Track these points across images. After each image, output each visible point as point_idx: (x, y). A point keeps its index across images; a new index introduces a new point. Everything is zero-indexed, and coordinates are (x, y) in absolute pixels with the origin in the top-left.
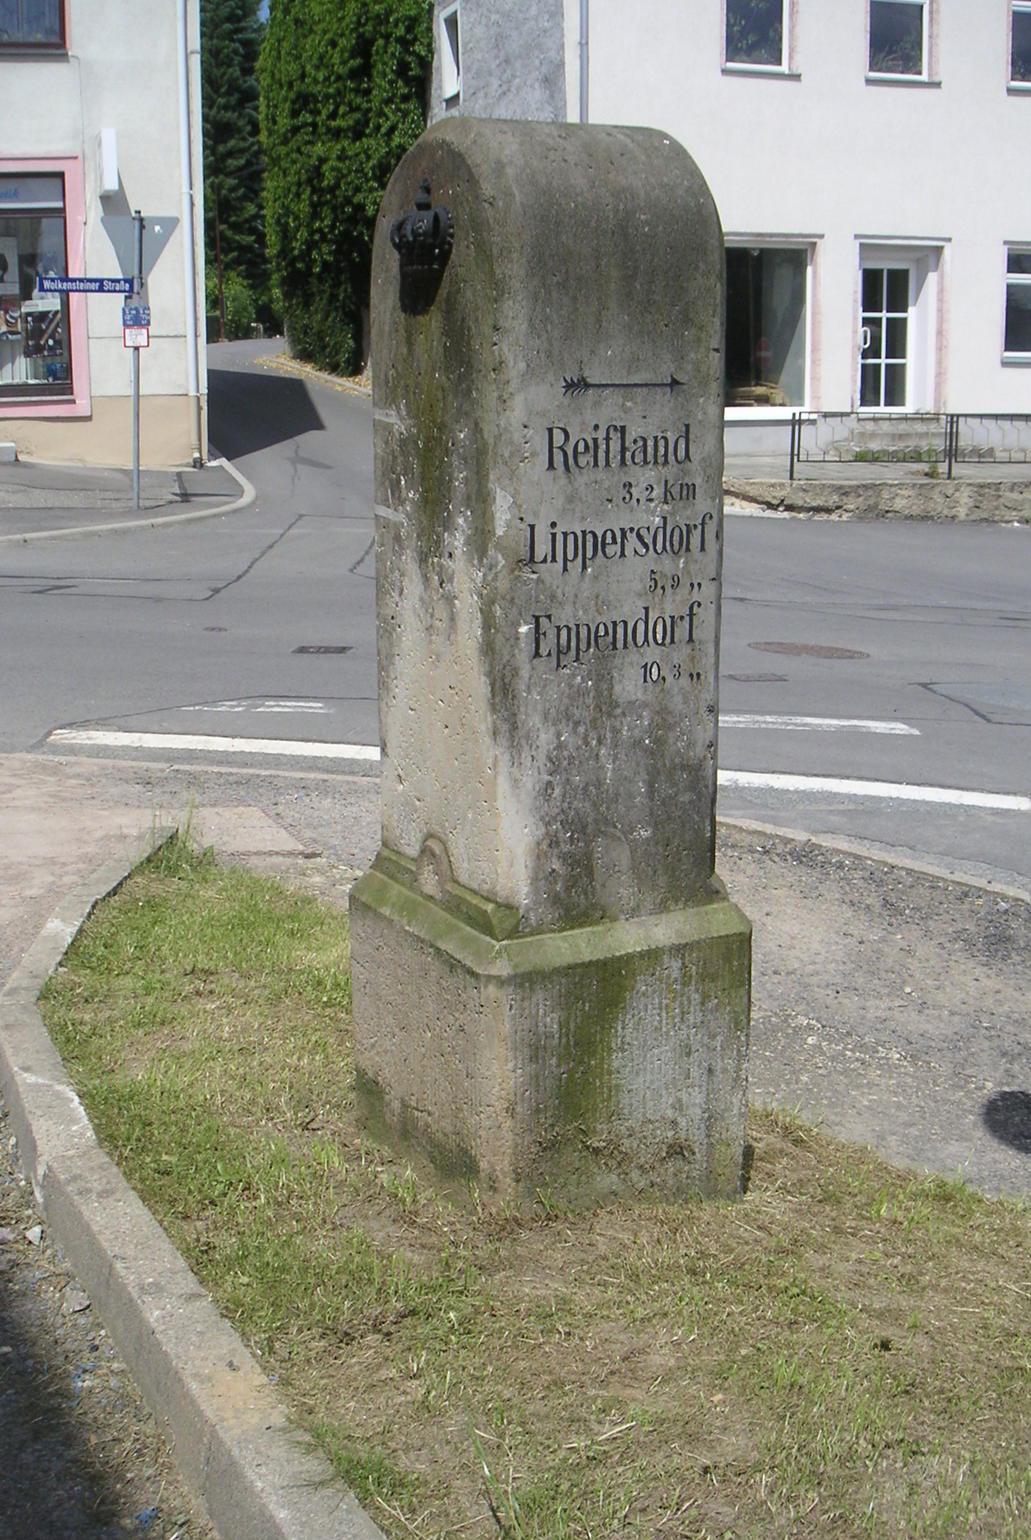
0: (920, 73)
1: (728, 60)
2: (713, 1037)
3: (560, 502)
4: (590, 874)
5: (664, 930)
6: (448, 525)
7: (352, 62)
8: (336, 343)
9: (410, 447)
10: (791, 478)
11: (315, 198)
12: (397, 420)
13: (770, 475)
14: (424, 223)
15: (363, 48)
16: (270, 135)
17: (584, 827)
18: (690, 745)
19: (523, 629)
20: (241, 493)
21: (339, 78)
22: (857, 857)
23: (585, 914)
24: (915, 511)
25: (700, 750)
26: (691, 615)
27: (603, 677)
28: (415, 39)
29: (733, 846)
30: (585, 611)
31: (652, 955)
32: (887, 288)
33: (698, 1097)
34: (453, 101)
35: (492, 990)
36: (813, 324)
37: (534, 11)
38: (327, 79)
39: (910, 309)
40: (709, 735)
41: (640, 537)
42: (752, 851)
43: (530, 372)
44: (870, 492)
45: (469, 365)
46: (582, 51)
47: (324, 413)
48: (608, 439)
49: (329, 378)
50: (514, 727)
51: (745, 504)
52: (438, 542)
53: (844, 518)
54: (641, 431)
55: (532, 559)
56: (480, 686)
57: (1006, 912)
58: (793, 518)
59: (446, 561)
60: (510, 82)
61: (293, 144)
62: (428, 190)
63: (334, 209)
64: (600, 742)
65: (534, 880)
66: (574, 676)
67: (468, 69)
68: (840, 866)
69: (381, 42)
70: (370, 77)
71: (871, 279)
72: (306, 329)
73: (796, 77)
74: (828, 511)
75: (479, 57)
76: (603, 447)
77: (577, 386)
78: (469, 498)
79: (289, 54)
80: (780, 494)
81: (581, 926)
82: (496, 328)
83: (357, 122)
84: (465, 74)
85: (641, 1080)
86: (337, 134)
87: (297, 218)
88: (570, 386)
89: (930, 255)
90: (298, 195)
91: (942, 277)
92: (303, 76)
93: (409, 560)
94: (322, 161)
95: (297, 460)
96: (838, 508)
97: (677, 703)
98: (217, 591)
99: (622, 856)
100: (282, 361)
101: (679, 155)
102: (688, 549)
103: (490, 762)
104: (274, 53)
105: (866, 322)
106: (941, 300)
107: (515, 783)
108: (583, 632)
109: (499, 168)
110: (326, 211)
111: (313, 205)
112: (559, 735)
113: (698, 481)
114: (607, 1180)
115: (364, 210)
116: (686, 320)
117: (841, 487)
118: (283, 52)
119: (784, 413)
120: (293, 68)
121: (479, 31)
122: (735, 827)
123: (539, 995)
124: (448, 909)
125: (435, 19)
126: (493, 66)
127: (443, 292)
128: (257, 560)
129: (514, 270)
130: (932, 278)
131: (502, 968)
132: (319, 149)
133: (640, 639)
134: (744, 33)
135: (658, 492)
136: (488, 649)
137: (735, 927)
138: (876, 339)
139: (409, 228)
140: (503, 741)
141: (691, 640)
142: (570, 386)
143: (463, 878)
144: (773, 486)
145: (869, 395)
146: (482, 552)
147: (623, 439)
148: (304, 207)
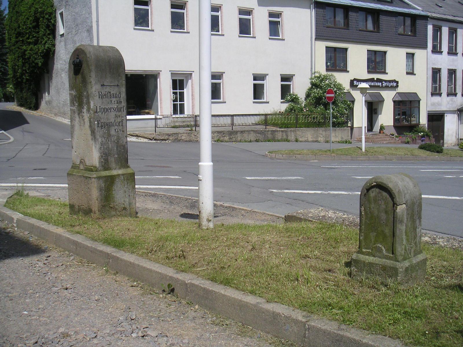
0: (184, 30)
1: (135, 26)
2: (129, 190)
3: (101, 103)
4: (108, 162)
5: (120, 172)
6: (83, 108)
7: (33, 24)
8: (31, 101)
9: (76, 96)
10: (155, 132)
11: (23, 61)
12: (74, 93)
13: (151, 132)
14: (78, 61)
15: (37, 20)
16: (9, 43)
17: (107, 154)
18: (123, 142)
19: (96, 123)
20: (10, 139)
21: (30, 28)
22: (165, 195)
23: (107, 168)
24: (187, 139)
25: (124, 143)
26: (122, 121)
27: (109, 131)
28: (51, 19)
29: (139, 195)
30: (105, 120)
31: (119, 175)
32: (178, 84)
33: (127, 200)
34: (62, 35)
35: (93, 180)
36: (160, 94)
37: (84, 12)
38: (26, 28)
39: (185, 89)
40: (126, 141)
41: (114, 109)
42: (142, 195)
43: (96, 83)
44: (176, 135)
45: (86, 83)
46: (97, 23)
47: (29, 120)
48: (108, 94)
49: (29, 111)
50: (95, 138)
51: (144, 139)
52: (81, 111)
53: (169, 142)
54: (113, 93)
55: (97, 112)
56: (89, 132)
57: (195, 202)
58: (156, 142)
59: (83, 114)
60: (78, 31)
61: (17, 46)
62: (78, 56)
63: (29, 64)
64: (108, 141)
65: (99, 163)
66: (104, 130)
67: (66, 27)
68: (161, 197)
69: (41, 19)
70: (39, 28)
71: (174, 82)
72: (22, 98)
73: (153, 31)
74: (165, 140)
75: (69, 24)
76: (107, 95)
77: (103, 85)
78: (86, 103)
79: (15, 21)
80: (153, 136)
81: (107, 170)
82: (90, 77)
83: (35, 40)
84: (66, 28)
85: (118, 196)
86: (29, 43)
87: (18, 66)
88: (102, 85)
89: (189, 75)
90: (18, 60)
91: (192, 81)
92: (19, 27)
93: (76, 115)
94: (25, 51)
95: (23, 131)
96: (168, 139)
97: (120, 135)
98: (9, 160)
99: (113, 159)
100: (14, 107)
101: (117, 51)
103: (91, 144)
104: (10, 20)
105: (174, 93)
106: (192, 87)
107: (96, 147)
108: (105, 123)
109: (90, 52)
110: (27, 65)
111: (23, 63)
112: (102, 139)
113: (122, 101)
114: (113, 213)
115: (38, 64)
116: (119, 76)
117: (168, 134)
118: (13, 20)
119: (153, 117)
120: (16, 25)
121: (69, 17)
122: (139, 191)
123: (101, 180)
124: (85, 170)
125: (57, 13)
126: (73, 26)
127: (81, 71)
128: (17, 153)
129: (93, 68)
130: (190, 81)
131: (95, 176)
132: (24, 47)
133: (114, 125)
134: (139, 19)
135: (116, 102)
136: (90, 126)
137: (132, 172)
138: (176, 98)
139: (75, 61)
140: (93, 140)
141: (122, 125)
142: (102, 85)
143: (87, 164)
144: (151, 134)
145: (175, 112)
146: (89, 111)
147: (110, 94)
148: (20, 63)
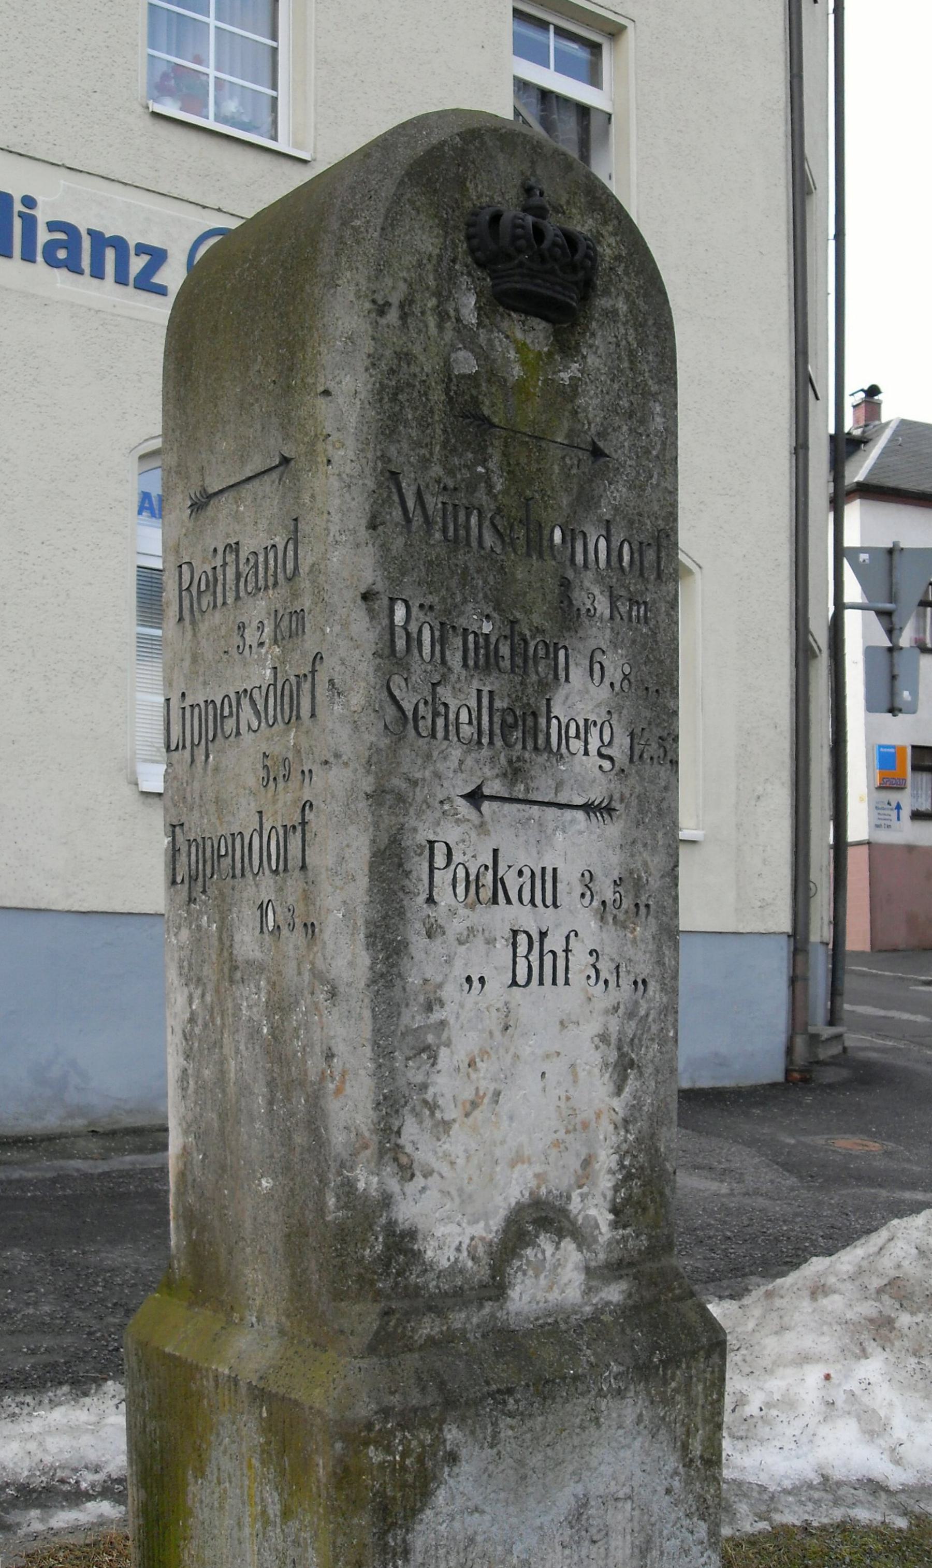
102: (298, 717)
